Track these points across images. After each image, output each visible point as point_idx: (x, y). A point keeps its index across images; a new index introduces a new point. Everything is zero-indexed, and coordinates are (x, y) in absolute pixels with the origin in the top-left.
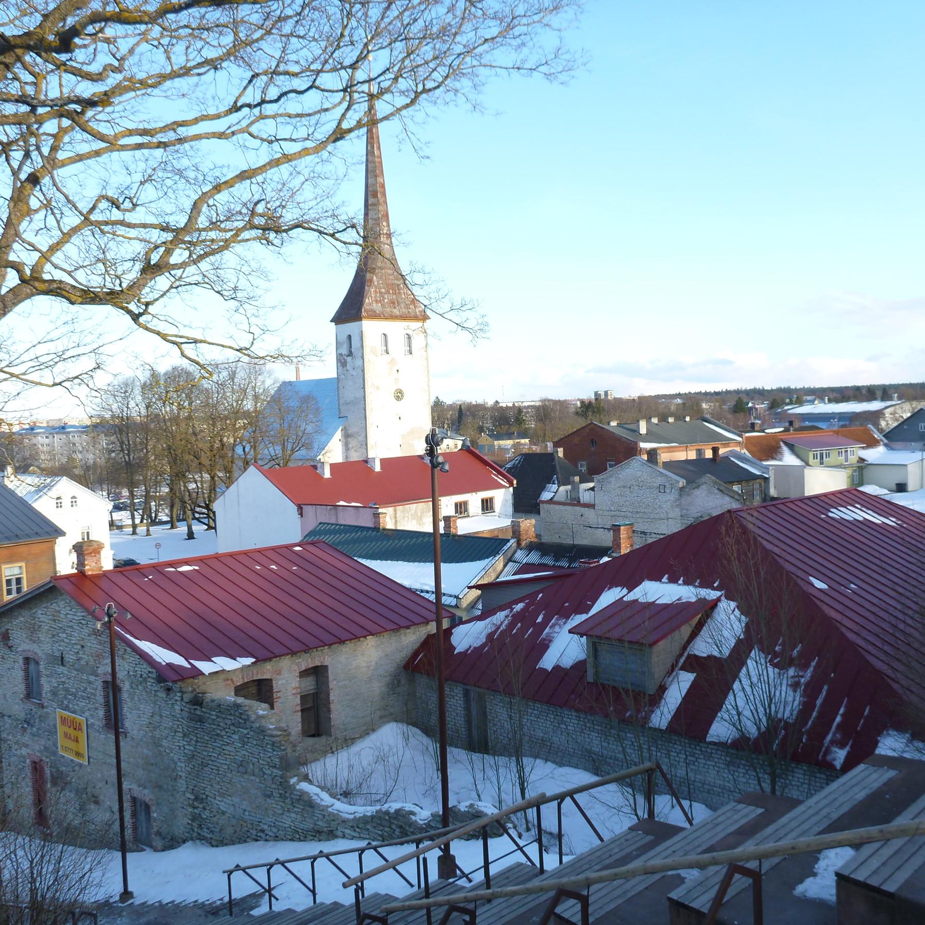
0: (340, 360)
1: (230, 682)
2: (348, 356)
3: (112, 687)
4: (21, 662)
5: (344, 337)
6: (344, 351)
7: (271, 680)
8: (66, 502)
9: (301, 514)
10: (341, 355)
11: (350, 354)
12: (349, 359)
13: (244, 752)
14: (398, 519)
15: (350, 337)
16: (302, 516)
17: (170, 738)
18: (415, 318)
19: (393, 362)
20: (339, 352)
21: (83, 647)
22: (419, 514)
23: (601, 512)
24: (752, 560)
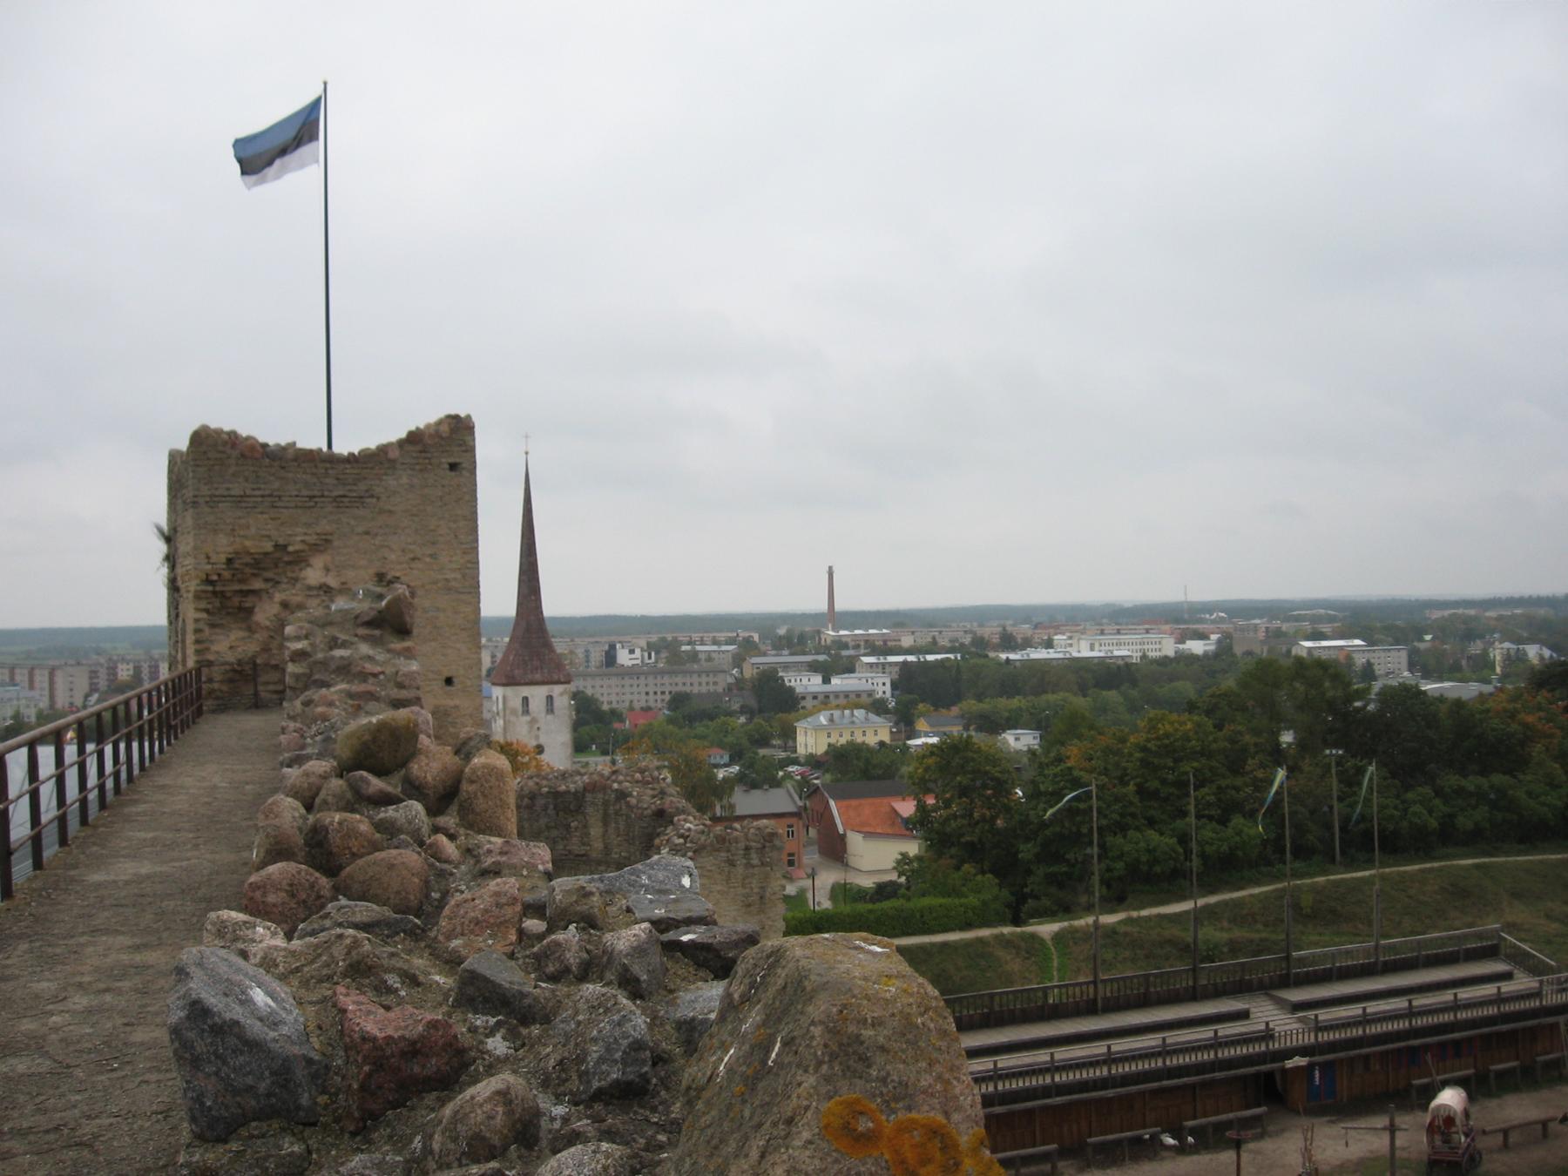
16: (830, 568)
19: (534, 721)
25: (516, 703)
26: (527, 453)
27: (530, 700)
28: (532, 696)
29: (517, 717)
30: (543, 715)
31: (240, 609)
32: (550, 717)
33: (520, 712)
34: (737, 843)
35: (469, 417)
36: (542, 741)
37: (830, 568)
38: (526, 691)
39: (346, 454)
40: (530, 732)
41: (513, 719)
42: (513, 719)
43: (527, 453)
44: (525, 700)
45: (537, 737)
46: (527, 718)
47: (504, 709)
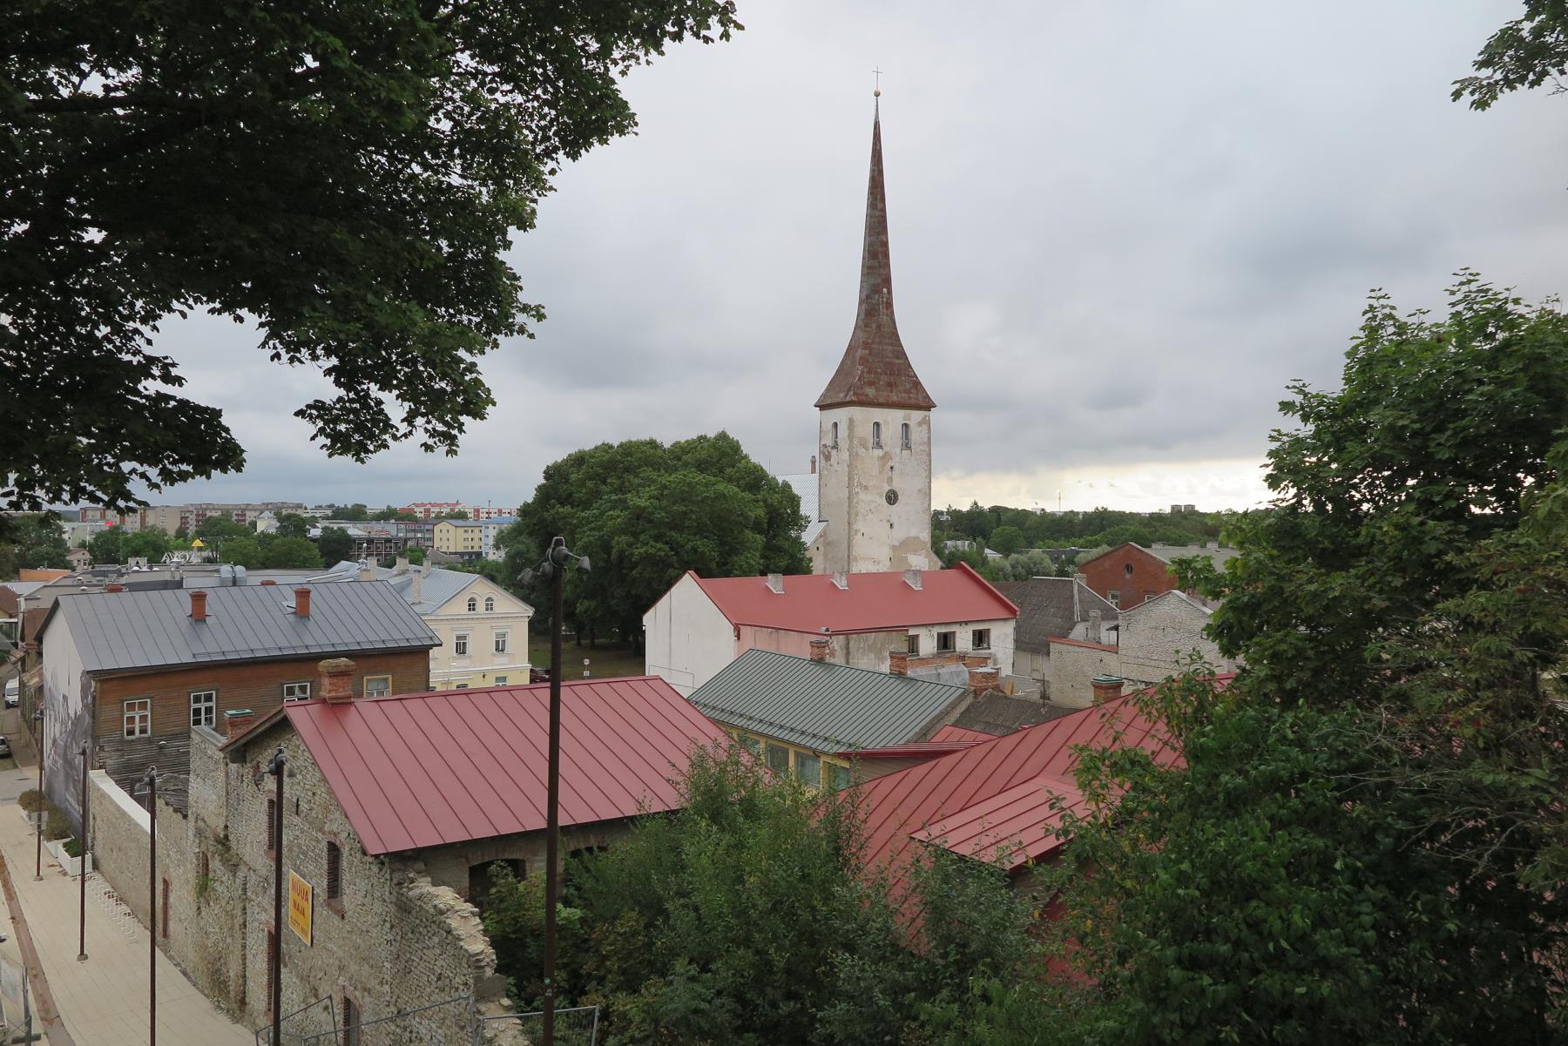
0: (824, 454)
1: (463, 860)
2: (833, 448)
3: (334, 851)
4: (266, 804)
5: (828, 426)
6: (829, 441)
7: (524, 861)
8: (481, 606)
9: (738, 637)
10: (825, 446)
11: (835, 446)
12: (834, 452)
13: (444, 964)
14: (851, 650)
15: (836, 425)
16: (739, 639)
17: (380, 927)
18: (919, 408)
19: (886, 457)
20: (823, 443)
21: (314, 794)
22: (879, 646)
23: (1126, 658)
24: (1451, 726)
25: (866, 431)
26: (877, 95)
27: (883, 428)
28: (887, 422)
29: (867, 449)
30: (898, 450)
31: (1161, 1003)
32: (905, 453)
33: (871, 445)
34: (207, 947)
35: (388, 507)
36: (896, 486)
37: (739, 639)
38: (877, 414)
39: (1168, 510)
40: (881, 472)
41: (861, 451)
42: (861, 451)
43: (877, 95)
44: (877, 425)
45: (890, 480)
46: (879, 452)
47: (851, 437)
